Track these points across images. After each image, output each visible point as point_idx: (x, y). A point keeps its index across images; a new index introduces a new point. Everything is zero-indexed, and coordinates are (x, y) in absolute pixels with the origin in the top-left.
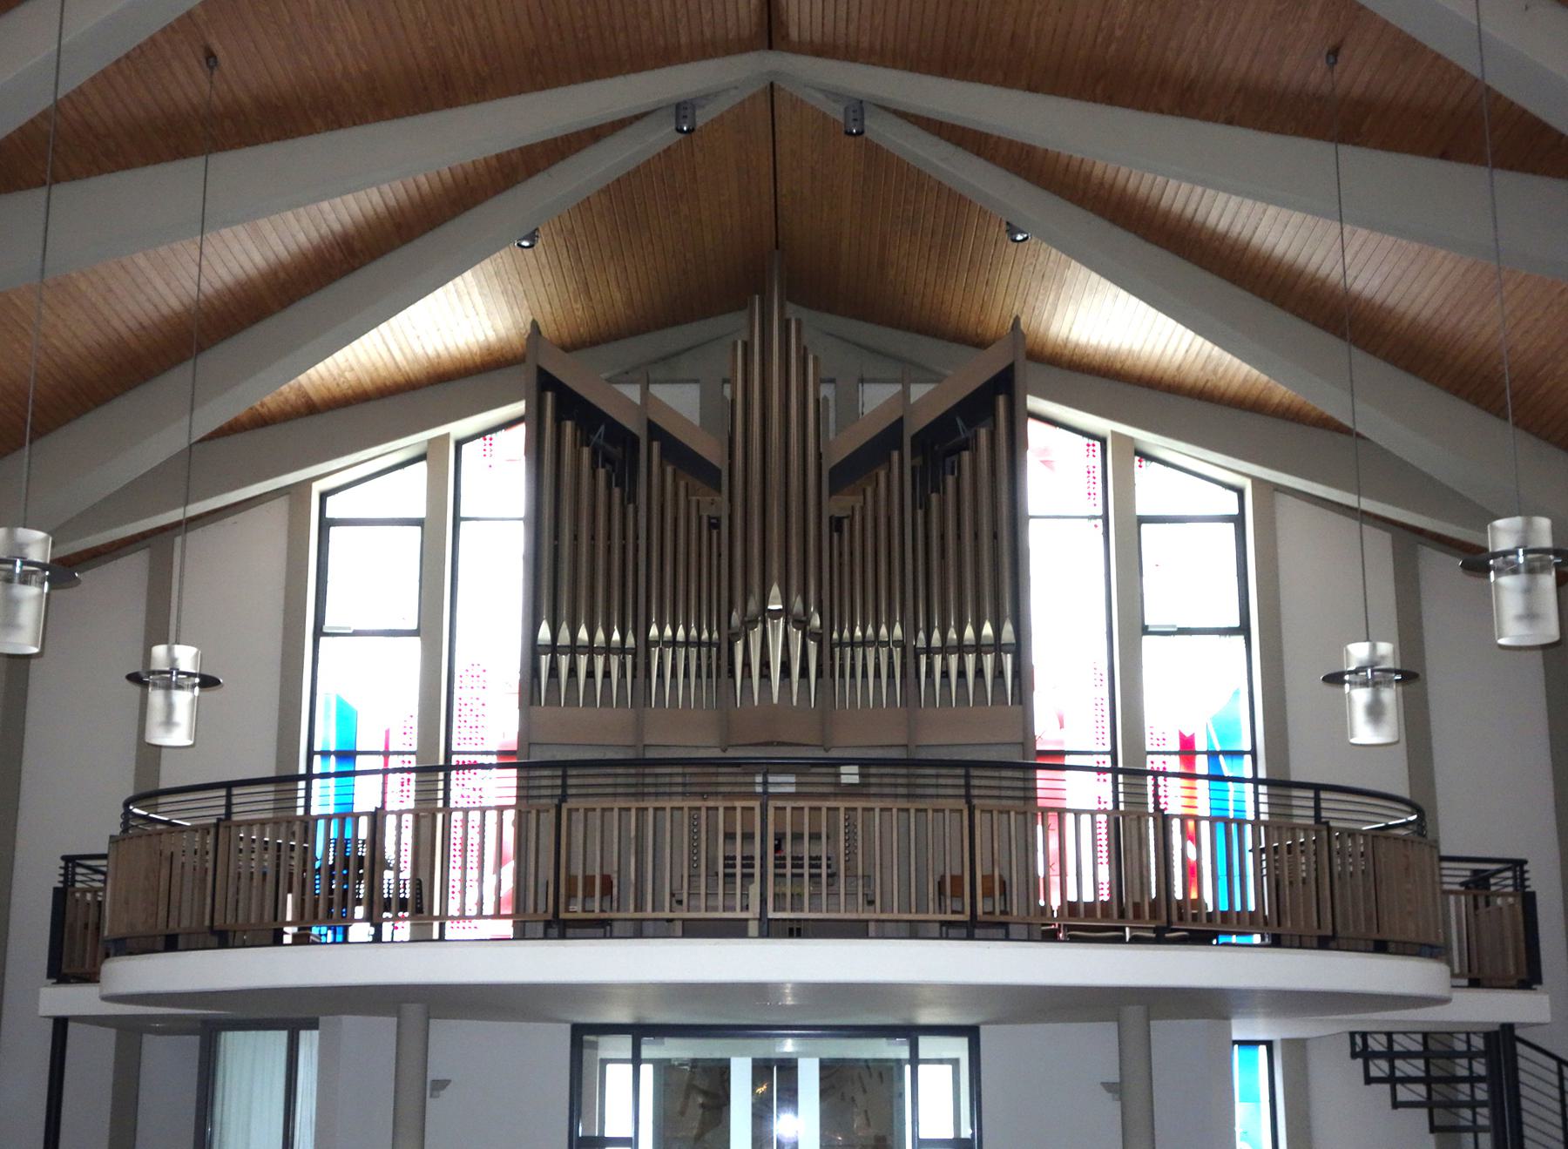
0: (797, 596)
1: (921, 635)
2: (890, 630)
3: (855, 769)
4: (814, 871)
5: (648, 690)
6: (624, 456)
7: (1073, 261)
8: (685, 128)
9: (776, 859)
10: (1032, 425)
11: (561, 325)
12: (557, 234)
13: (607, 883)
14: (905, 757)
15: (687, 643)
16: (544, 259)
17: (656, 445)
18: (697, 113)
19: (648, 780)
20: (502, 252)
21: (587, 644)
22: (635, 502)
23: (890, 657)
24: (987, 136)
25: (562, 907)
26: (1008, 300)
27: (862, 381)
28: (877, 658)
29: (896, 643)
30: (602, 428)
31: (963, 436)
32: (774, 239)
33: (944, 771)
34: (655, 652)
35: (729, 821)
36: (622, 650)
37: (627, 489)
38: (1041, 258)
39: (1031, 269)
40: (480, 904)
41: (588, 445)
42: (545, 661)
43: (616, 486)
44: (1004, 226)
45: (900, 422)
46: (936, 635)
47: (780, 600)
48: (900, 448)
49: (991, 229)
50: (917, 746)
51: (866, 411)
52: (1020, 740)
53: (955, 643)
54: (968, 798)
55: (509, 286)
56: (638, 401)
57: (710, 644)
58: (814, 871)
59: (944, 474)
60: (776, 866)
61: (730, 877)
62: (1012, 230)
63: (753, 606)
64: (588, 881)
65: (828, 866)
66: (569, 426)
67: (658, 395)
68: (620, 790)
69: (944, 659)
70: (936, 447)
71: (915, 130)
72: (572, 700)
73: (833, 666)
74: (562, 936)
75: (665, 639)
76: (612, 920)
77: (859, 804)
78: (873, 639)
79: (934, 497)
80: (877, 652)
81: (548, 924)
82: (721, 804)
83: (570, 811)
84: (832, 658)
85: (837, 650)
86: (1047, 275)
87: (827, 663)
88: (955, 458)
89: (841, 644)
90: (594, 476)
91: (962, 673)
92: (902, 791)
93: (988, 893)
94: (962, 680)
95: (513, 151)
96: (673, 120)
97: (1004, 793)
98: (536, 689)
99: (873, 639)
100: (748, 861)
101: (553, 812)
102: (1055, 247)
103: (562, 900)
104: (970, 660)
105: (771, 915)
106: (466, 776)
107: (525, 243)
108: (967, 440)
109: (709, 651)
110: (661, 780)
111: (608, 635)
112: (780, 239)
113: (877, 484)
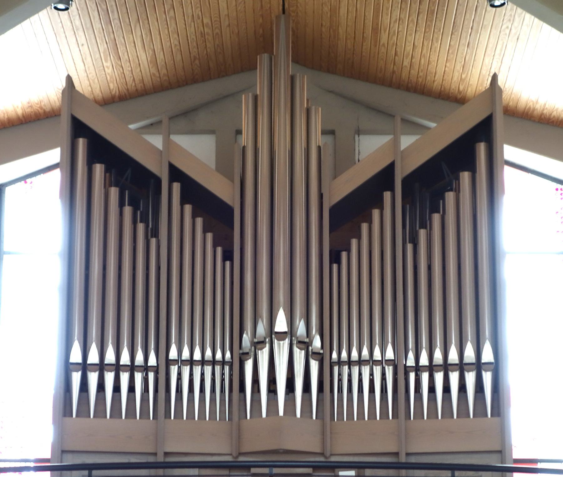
1: (411, 355)
2: (383, 351)
11: (93, 81)
16: (78, 22)
17: (176, 186)
26: (487, 60)
27: (359, 132)
29: (389, 362)
30: (129, 172)
32: (281, 8)
34: (174, 370)
37: (150, 226)
38: (516, 24)
39: (507, 31)
43: (141, 222)
45: (391, 167)
48: (392, 189)
51: (363, 156)
56: (160, 147)
79: (422, 233)
85: (336, 369)
89: (340, 363)
112: (286, 6)
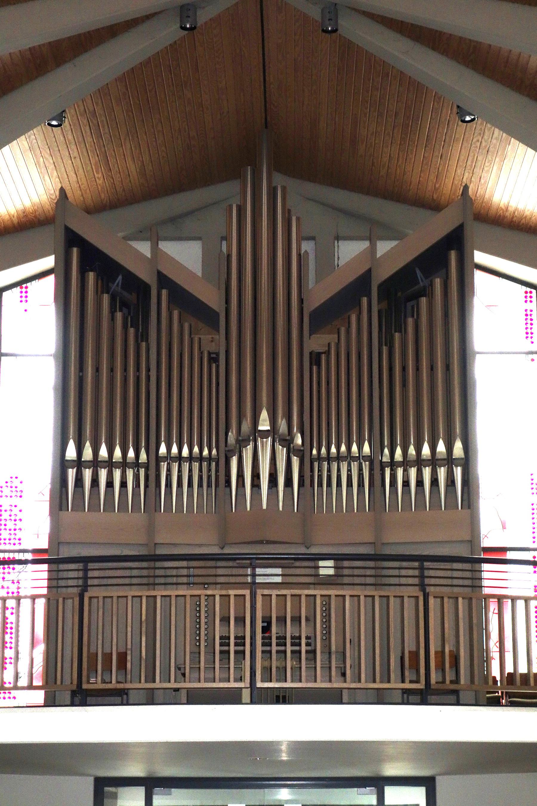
0: (282, 420)
1: (386, 451)
2: (360, 447)
3: (330, 563)
4: (226, 648)
5: (158, 496)
6: (138, 300)
7: (513, 139)
8: (188, 26)
9: (263, 638)
10: (478, 275)
12: (81, 115)
13: (122, 658)
14: (373, 553)
15: (191, 458)
16: (70, 137)
17: (164, 292)
18: (198, 13)
19: (158, 572)
20: (35, 130)
21: (107, 459)
22: (147, 341)
23: (360, 469)
24: (441, 34)
25: (84, 679)
27: (338, 238)
28: (349, 470)
29: (365, 458)
30: (120, 277)
31: (421, 284)
32: (263, 120)
33: (405, 564)
34: (164, 466)
35: (225, 605)
36: (136, 464)
39: (478, 144)
40: (17, 677)
41: (108, 293)
42: (71, 473)
43: (131, 326)
44: (455, 109)
46: (399, 452)
47: (268, 422)
49: (444, 110)
50: (383, 544)
51: (342, 263)
52: (468, 538)
53: (415, 458)
54: (422, 586)
55: (41, 159)
57: (210, 458)
58: (226, 648)
59: (405, 317)
60: (263, 645)
61: (225, 654)
62: (461, 112)
63: (246, 427)
64: (108, 657)
65: (308, 644)
66: (91, 276)
67: (165, 250)
68: (135, 581)
69: (405, 470)
70: (399, 294)
71: (382, 28)
72: (94, 506)
73: (312, 477)
74: (84, 703)
75: (172, 455)
76: (128, 689)
77: (332, 592)
78: (346, 454)
79: (397, 335)
80: (349, 465)
81: (73, 693)
82: (217, 592)
83: (90, 598)
84: (312, 470)
85: (316, 464)
86: (491, 149)
87: (307, 474)
88: (413, 303)
89: (319, 458)
90: (113, 318)
91: (420, 483)
92: (369, 580)
93: (441, 667)
94: (434, 488)
95: (44, 45)
96: (178, 19)
97: (455, 582)
98: (64, 497)
99: (346, 454)
100: (240, 640)
101: (77, 600)
102: (498, 128)
103: (85, 673)
104: (427, 472)
105: (259, 685)
106: (6, 570)
107: (54, 123)
108: (425, 288)
109: (209, 465)
110: (169, 572)
111: (125, 453)
112: (269, 118)
113: (349, 323)
